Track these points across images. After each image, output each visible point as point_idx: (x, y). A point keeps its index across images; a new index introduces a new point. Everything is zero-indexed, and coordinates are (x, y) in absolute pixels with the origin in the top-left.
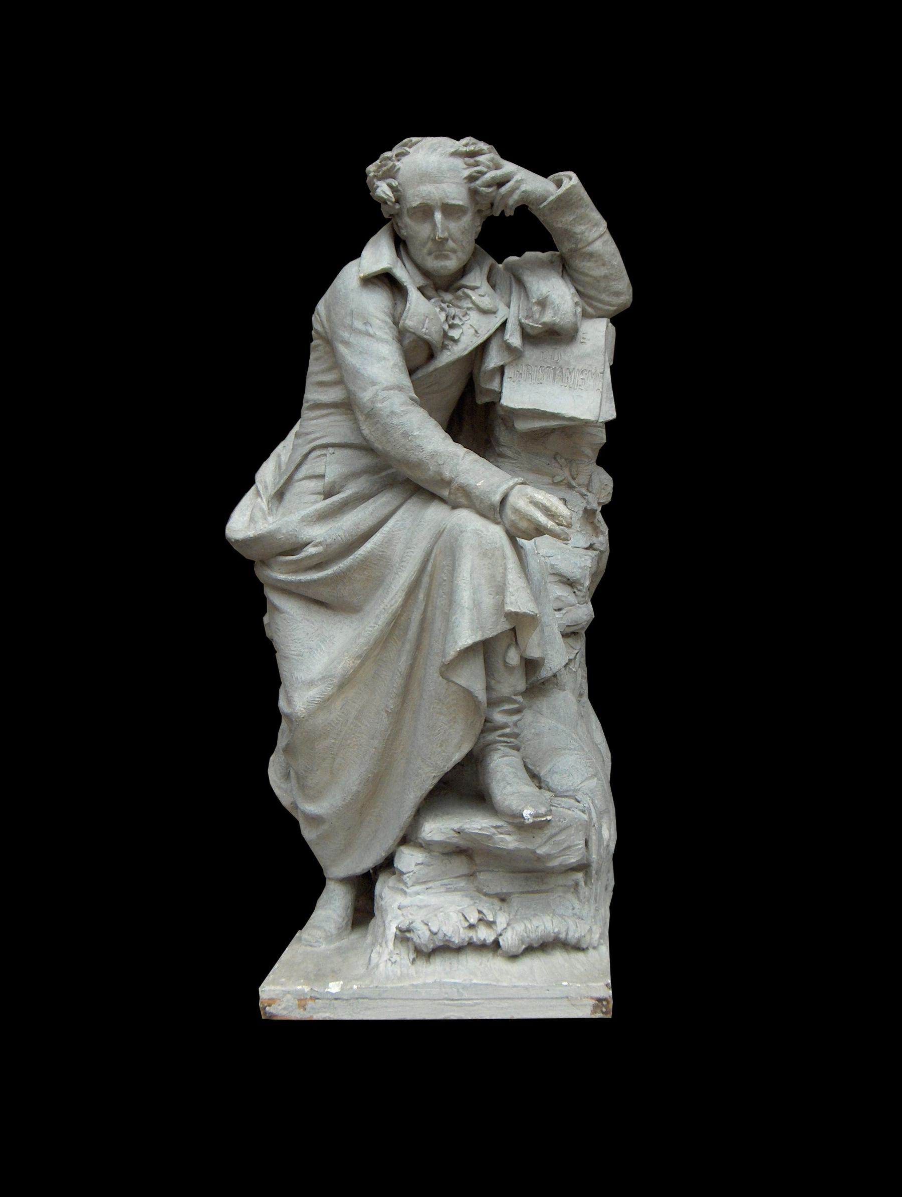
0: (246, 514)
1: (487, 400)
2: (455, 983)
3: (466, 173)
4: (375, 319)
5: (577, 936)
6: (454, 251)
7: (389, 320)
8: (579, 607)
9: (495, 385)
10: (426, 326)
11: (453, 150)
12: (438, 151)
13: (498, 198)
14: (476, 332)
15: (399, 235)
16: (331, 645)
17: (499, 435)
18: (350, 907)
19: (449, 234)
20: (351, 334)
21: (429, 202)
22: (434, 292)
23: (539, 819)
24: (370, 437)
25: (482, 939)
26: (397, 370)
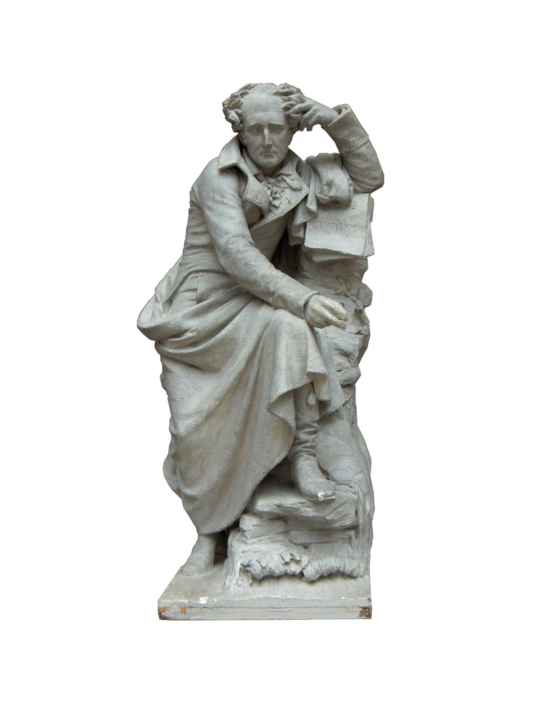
1: (296, 243)
2: (276, 598)
4: (228, 194)
5: (350, 569)
6: (276, 153)
7: (236, 195)
8: (352, 369)
9: (301, 234)
10: (259, 198)
12: (266, 92)
14: (289, 202)
15: (243, 143)
17: (303, 265)
18: (213, 551)
19: (273, 143)
20: (213, 203)
21: (261, 123)
22: (264, 178)
23: (327, 498)
24: (225, 266)
25: (293, 571)
26: (241, 225)
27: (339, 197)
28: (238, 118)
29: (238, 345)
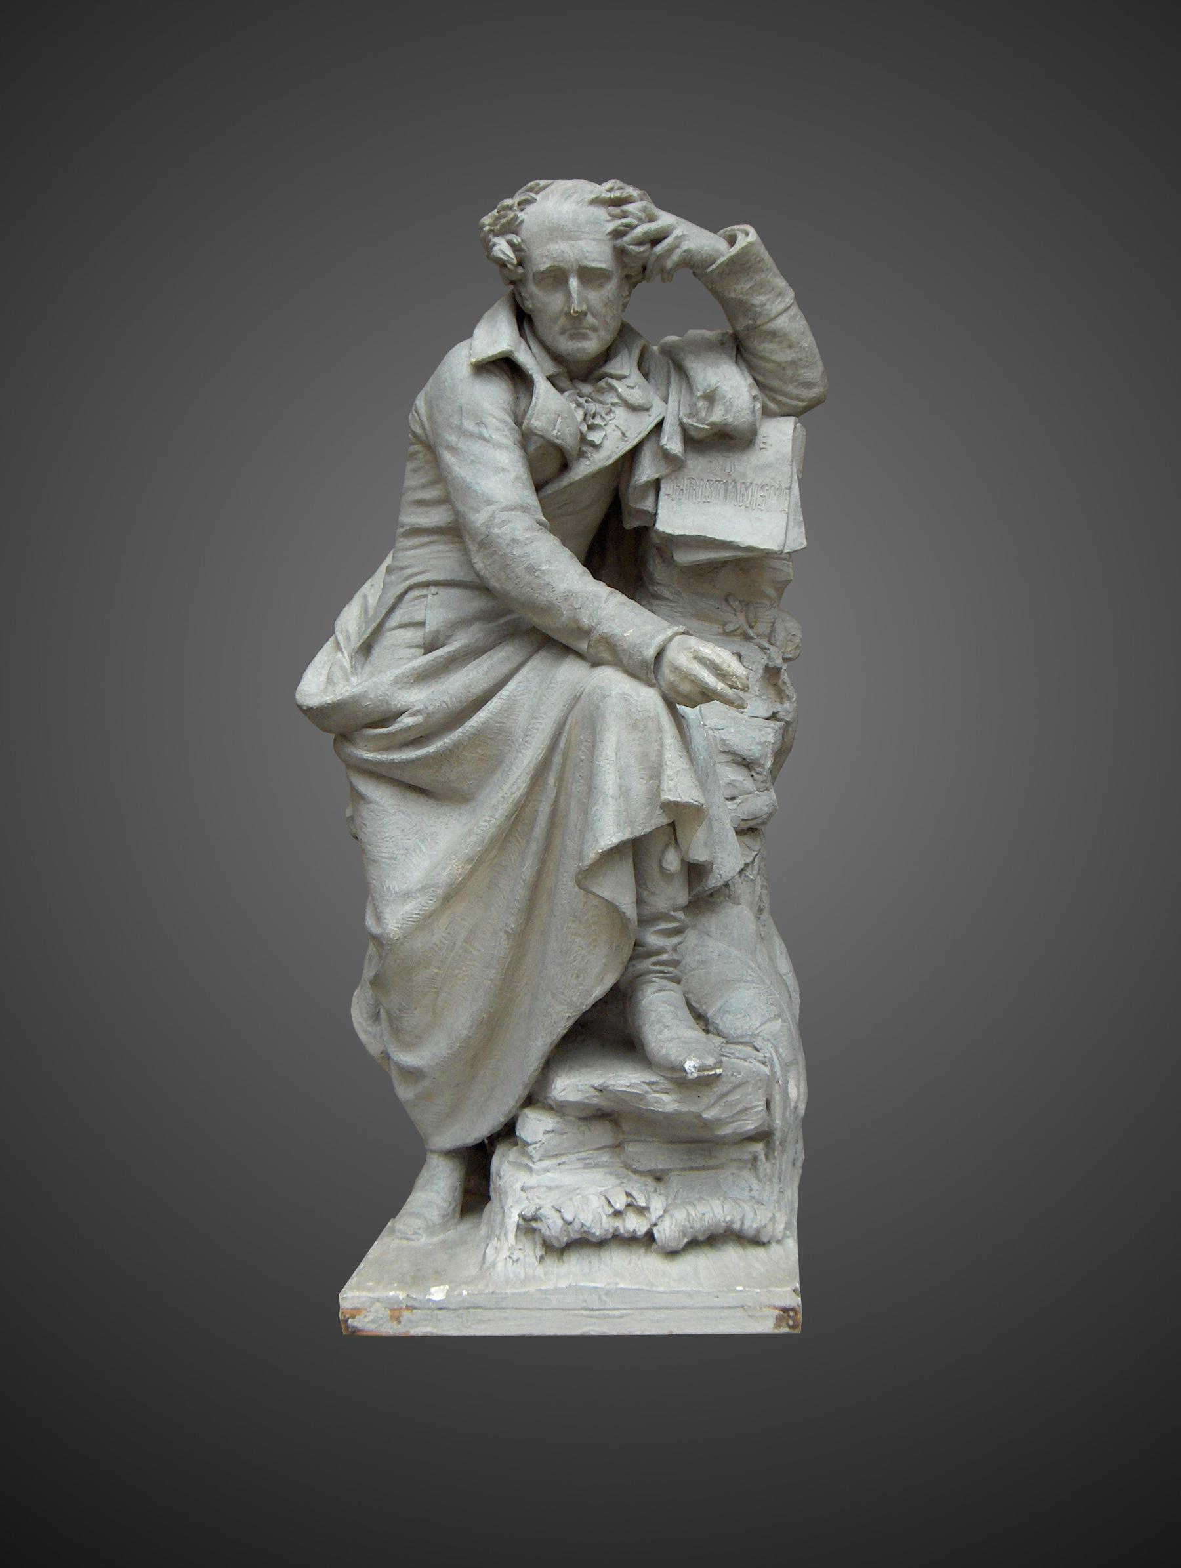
1: (637, 523)
2: (595, 1288)
3: (611, 226)
4: (491, 418)
5: (755, 1225)
6: (595, 329)
7: (509, 420)
8: (758, 795)
9: (648, 505)
10: (558, 427)
11: (593, 196)
12: (573, 198)
13: (652, 259)
14: (624, 434)
15: (523, 308)
16: (433, 844)
17: (653, 570)
18: (458, 1187)
20: (460, 438)
21: (561, 264)
22: (568, 383)
23: (706, 1073)
24: (484, 573)
25: (632, 1230)
26: (520, 485)
27: (730, 425)
28: (512, 255)
29: (513, 742)
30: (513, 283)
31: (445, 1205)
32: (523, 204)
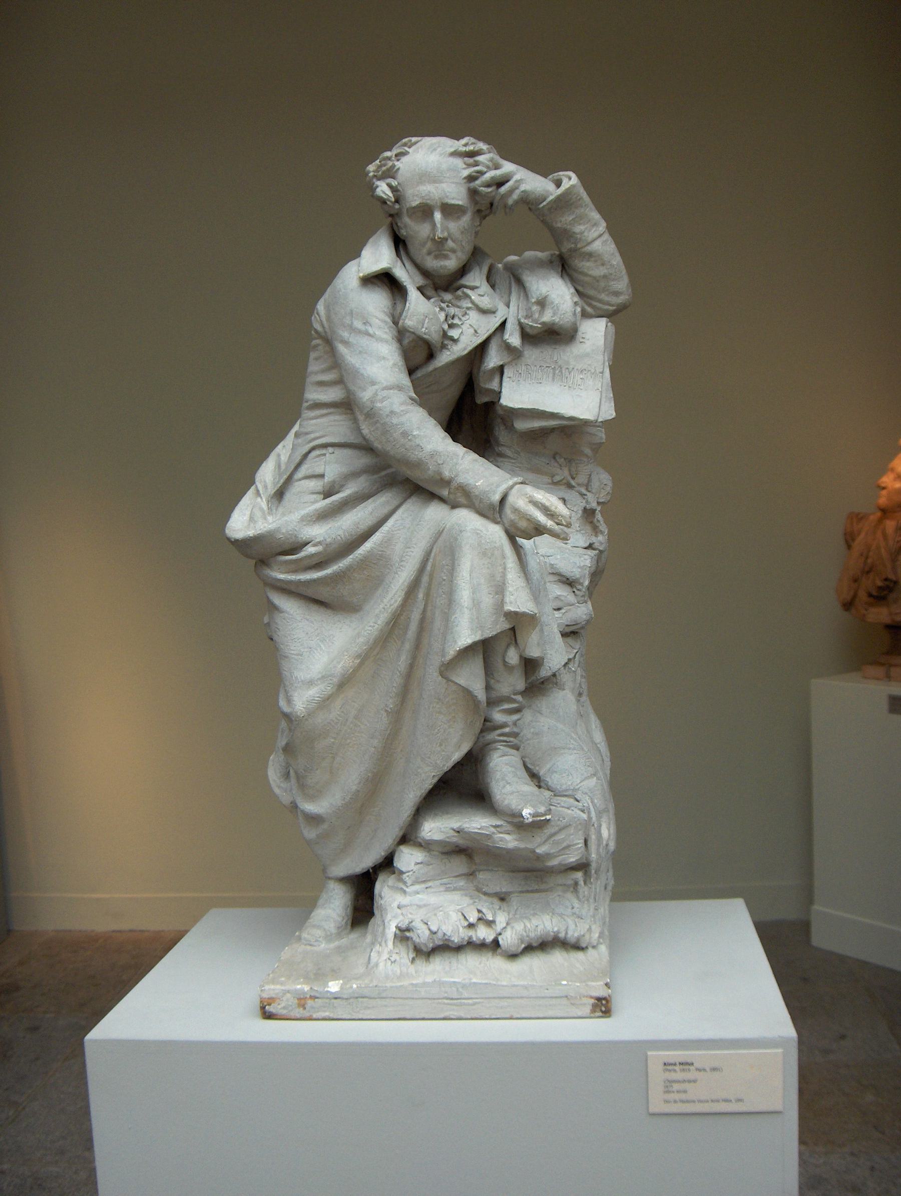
0: (245, 514)
1: (486, 399)
2: (454, 982)
3: (466, 173)
4: (375, 319)
5: (576, 935)
6: (454, 251)
7: (389, 320)
8: (578, 606)
9: (494, 385)
10: (425, 325)
11: (452, 150)
12: (437, 151)
13: (498, 198)
14: (476, 331)
15: (399, 235)
16: (331, 644)
17: (498, 435)
18: (350, 906)
19: (449, 234)
20: (351, 334)
21: (428, 202)
22: (434, 292)
23: (538, 819)
24: (369, 437)
25: (482, 938)
26: (397, 370)
27: (557, 324)
28: (391, 194)
30: (391, 216)
31: (340, 919)
32: (399, 156)
